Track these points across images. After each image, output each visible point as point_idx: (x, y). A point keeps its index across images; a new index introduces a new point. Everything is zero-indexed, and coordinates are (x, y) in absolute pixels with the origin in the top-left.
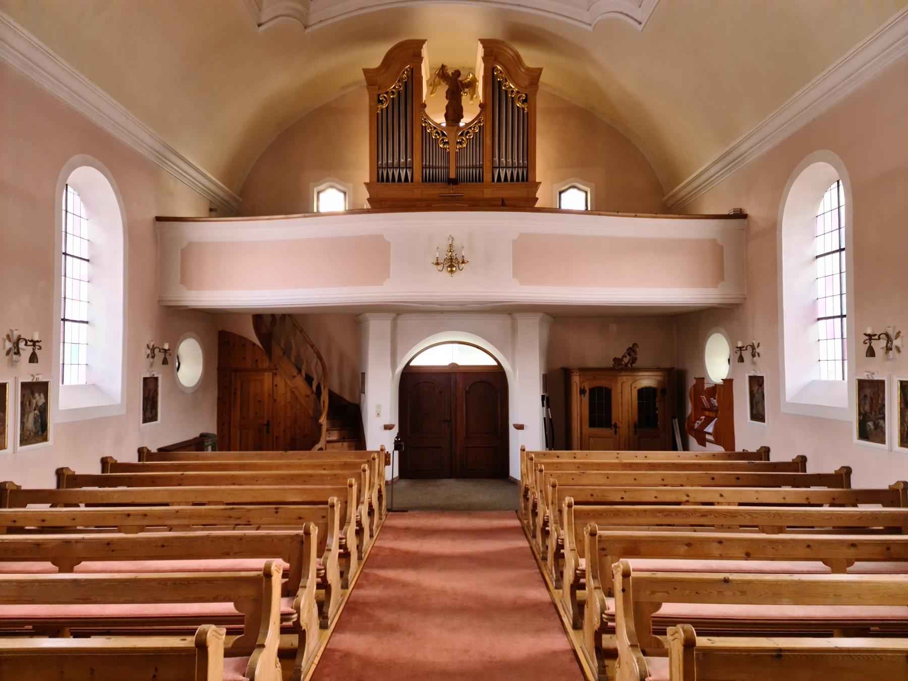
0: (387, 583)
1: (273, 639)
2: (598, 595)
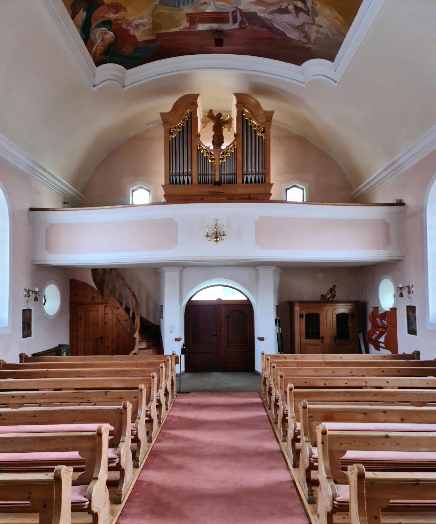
0: (176, 438)
1: (103, 474)
2: (308, 446)
